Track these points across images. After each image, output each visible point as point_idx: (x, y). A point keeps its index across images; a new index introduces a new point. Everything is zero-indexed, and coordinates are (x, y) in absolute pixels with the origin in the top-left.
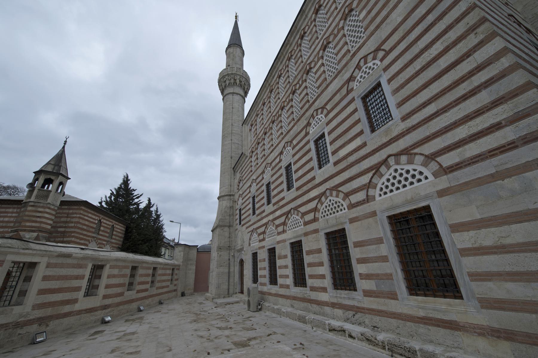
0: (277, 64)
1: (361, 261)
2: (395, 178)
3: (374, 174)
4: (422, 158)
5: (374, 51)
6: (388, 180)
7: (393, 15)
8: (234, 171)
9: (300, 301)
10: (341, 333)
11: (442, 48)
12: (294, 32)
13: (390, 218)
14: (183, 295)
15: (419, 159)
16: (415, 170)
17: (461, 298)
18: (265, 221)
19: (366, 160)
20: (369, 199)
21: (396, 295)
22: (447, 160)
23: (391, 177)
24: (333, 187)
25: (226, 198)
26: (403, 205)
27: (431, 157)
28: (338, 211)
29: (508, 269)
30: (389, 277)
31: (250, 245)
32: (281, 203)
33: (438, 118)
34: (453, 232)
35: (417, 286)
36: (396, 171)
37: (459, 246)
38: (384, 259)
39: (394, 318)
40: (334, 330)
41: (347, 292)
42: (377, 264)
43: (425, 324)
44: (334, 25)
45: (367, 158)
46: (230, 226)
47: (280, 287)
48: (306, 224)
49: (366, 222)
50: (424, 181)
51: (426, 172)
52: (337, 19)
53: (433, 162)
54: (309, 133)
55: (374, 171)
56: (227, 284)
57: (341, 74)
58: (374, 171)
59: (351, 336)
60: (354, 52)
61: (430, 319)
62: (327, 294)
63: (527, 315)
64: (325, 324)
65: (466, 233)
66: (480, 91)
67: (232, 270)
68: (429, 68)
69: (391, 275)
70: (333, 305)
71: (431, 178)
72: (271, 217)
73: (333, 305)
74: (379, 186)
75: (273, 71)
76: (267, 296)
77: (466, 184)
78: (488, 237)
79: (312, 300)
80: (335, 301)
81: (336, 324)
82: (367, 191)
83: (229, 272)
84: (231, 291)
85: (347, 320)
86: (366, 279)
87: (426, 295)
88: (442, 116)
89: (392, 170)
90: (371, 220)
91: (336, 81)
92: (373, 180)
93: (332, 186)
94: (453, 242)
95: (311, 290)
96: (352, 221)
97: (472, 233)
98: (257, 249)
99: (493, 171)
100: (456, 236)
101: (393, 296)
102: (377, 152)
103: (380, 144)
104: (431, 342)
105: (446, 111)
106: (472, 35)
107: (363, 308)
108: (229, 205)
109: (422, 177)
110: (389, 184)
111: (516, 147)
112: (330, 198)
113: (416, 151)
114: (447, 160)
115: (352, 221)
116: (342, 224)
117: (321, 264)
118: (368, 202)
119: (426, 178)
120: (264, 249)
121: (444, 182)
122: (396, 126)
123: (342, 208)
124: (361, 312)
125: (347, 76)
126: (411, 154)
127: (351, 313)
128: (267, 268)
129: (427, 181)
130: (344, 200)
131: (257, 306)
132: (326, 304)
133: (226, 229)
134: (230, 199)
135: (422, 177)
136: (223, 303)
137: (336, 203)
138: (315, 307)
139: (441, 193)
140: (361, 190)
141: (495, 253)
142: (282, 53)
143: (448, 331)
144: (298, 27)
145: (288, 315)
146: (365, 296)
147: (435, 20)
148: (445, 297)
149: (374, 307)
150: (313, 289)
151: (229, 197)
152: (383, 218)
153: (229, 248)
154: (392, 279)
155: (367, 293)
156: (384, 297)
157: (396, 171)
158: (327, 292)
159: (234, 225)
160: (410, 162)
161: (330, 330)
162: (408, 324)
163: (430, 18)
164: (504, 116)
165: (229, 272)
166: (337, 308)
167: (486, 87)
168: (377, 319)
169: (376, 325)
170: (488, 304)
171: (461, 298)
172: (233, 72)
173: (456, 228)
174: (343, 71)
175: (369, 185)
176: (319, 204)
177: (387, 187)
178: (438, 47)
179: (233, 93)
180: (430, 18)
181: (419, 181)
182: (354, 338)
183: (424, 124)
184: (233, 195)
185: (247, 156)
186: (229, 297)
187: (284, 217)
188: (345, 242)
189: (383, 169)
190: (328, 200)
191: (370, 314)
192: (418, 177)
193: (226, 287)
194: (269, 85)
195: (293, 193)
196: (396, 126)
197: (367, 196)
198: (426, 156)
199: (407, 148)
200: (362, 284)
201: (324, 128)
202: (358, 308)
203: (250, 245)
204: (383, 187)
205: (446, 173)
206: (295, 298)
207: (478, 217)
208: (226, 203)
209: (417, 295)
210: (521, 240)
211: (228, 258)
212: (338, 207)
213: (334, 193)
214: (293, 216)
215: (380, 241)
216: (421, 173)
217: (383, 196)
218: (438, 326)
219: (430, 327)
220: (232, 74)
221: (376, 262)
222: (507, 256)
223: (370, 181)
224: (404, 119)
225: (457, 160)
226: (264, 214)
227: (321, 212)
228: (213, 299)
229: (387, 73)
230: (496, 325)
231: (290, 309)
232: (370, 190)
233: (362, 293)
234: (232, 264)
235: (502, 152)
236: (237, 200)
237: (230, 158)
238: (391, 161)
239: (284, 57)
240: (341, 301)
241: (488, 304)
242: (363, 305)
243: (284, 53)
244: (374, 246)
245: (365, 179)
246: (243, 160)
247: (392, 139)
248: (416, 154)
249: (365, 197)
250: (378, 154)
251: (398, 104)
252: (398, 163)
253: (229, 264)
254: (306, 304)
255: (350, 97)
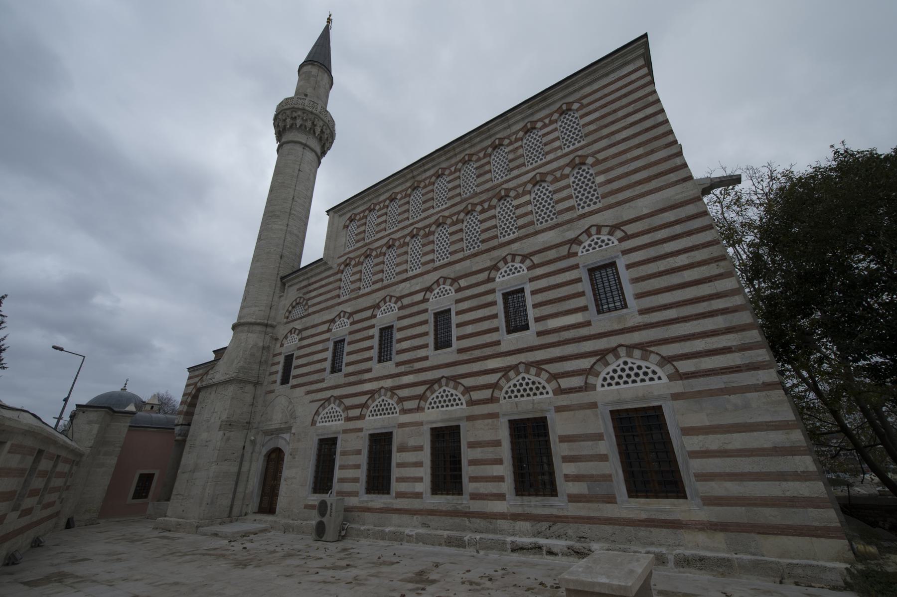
0: (439, 157)
1: (567, 459)
2: (442, 396)
3: (598, 360)
4: (658, 358)
5: (612, 227)
6: (515, 385)
7: (640, 202)
8: (284, 284)
9: (446, 516)
10: (534, 551)
11: (687, 262)
12: (482, 133)
13: (432, 429)
14: (69, 525)
15: (654, 358)
16: (648, 368)
17: (685, 497)
18: (368, 387)
19: (589, 342)
20: (588, 387)
21: (615, 498)
22: (685, 366)
23: (518, 384)
24: (532, 362)
25: (258, 328)
26: (443, 421)
27: (554, 377)
28: (438, 407)
29: (728, 470)
30: (607, 478)
31: (313, 423)
32: (418, 365)
33: (678, 325)
34: (683, 435)
35: (639, 486)
36: (524, 379)
37: (688, 449)
38: (603, 458)
39: (610, 524)
40: (522, 549)
41: (540, 498)
42: (592, 463)
43: (647, 526)
44: (555, 165)
45: (590, 339)
46: (257, 384)
47: (397, 497)
48: (348, 419)
49: (580, 414)
50: (657, 381)
51: (660, 372)
52: (563, 162)
53: (554, 381)
54: (428, 300)
55: (598, 357)
56: (231, 496)
57: (561, 229)
58: (598, 357)
59: (550, 553)
60: (584, 214)
61: (653, 521)
62: (505, 502)
63: (738, 508)
64: (504, 543)
65: (695, 437)
66: (717, 315)
67: (245, 469)
68: (673, 275)
69: (610, 476)
70: (515, 517)
71: (665, 380)
72: (389, 383)
73: (515, 517)
74: (603, 375)
75: (427, 163)
76: (357, 514)
77: (699, 392)
78: (714, 442)
79: (473, 513)
80: (519, 510)
81: (527, 540)
82: (587, 378)
83: (239, 474)
84: (236, 510)
85: (538, 534)
86: (572, 481)
87: (647, 497)
88: (682, 325)
89: (621, 361)
90: (588, 411)
91: (552, 233)
92: (596, 367)
93: (531, 360)
94: (683, 446)
95: (472, 499)
96: (559, 409)
97: (701, 437)
98: (460, 419)
99: (723, 386)
100: (686, 439)
101: (610, 499)
102: (605, 336)
103: (610, 329)
104: (652, 544)
105: (685, 321)
106: (714, 265)
107: (566, 517)
108: (261, 344)
109: (544, 391)
110: (515, 389)
111: (741, 371)
112: (383, 397)
113: (652, 349)
114: (685, 366)
115: (559, 409)
116: (542, 411)
117: (499, 462)
118: (586, 390)
119: (660, 378)
120: (360, 434)
121: (678, 387)
122: (631, 316)
123: (459, 402)
124: (562, 522)
125: (571, 235)
126: (647, 351)
127: (545, 525)
128: (365, 467)
129: (660, 381)
130: (548, 381)
131: (340, 532)
132: (502, 516)
133: (249, 388)
134: (266, 333)
135: (544, 391)
136: (238, 532)
137: (452, 395)
138: (479, 523)
139: (676, 397)
140: (579, 375)
141: (719, 457)
142: (454, 149)
143: (670, 531)
144: (492, 132)
145: (419, 539)
146: (570, 501)
147: (683, 233)
148: (667, 497)
149: (583, 513)
150: (475, 496)
151: (264, 329)
152: (604, 412)
153: (248, 425)
154: (612, 481)
155: (574, 498)
156: (598, 502)
157: (444, 391)
158: (505, 500)
159: (265, 383)
160: (644, 358)
161: (513, 550)
162: (627, 528)
163: (678, 229)
164: (734, 343)
165: (239, 474)
166: (521, 520)
167: (722, 314)
168: (585, 529)
169: (582, 534)
170: (710, 501)
171: (685, 497)
172: (314, 111)
173: (687, 431)
174: (565, 227)
175: (590, 372)
176: (370, 401)
177: (513, 391)
178: (682, 260)
179: (305, 146)
180: (678, 229)
181: (652, 379)
182: (556, 554)
183: (664, 325)
184: (273, 327)
185: (331, 268)
186: (231, 522)
187: (424, 388)
188: (546, 435)
189: (512, 374)
190: (441, 390)
191: (576, 522)
192: (651, 375)
193: (226, 502)
194: (413, 177)
195: (338, 378)
196: (631, 316)
197: (586, 383)
198: (662, 357)
199: (642, 344)
200: (565, 488)
201: (525, 283)
202: (557, 517)
203: (313, 423)
204: (608, 377)
205: (681, 379)
206: (432, 513)
207: (708, 424)
208: (254, 338)
209: (637, 497)
210: (739, 447)
211: (242, 444)
212: (538, 389)
213: (337, 401)
214: (332, 405)
215: (599, 437)
216: (654, 372)
217: (606, 388)
218: (661, 527)
219: (652, 529)
220: (312, 113)
221: (592, 461)
222: (728, 459)
223: (592, 367)
224: (642, 312)
225: (693, 369)
226: (367, 376)
227: (428, 402)
228: (197, 527)
229: (626, 257)
230: (714, 520)
231: (422, 531)
232: (590, 377)
233: (566, 498)
234: (247, 456)
235: (731, 372)
236: (281, 337)
237: (278, 257)
238: (622, 352)
239: (456, 155)
240: (528, 510)
241: (710, 501)
242: (566, 513)
243: (457, 150)
244: (590, 443)
245: (585, 363)
246: (317, 271)
247: (625, 329)
248: (652, 352)
249: (583, 384)
250: (605, 339)
251: (636, 295)
252: (629, 355)
253: (243, 455)
254: (457, 520)
255: (571, 261)
